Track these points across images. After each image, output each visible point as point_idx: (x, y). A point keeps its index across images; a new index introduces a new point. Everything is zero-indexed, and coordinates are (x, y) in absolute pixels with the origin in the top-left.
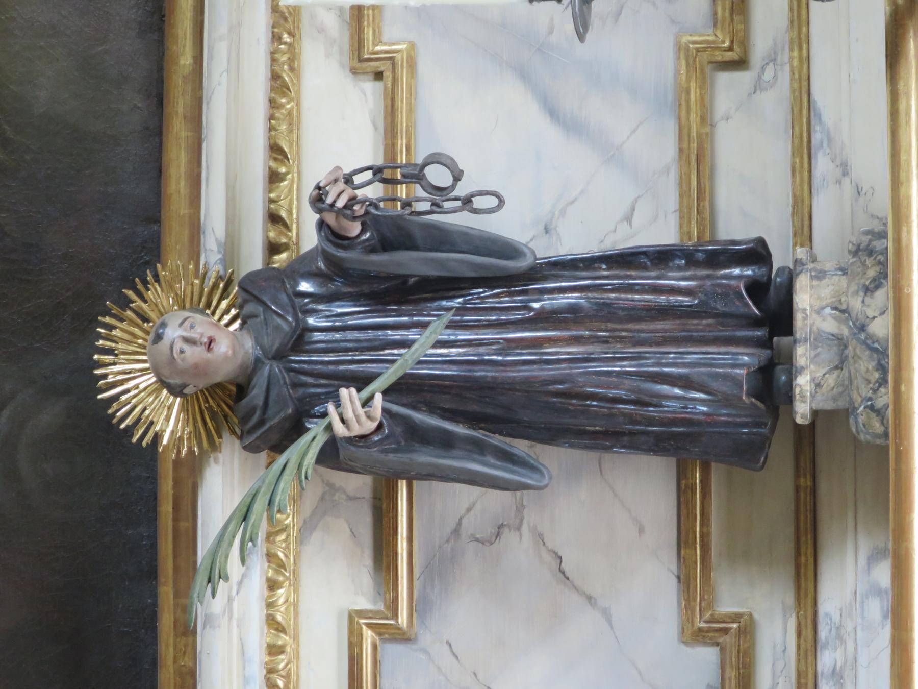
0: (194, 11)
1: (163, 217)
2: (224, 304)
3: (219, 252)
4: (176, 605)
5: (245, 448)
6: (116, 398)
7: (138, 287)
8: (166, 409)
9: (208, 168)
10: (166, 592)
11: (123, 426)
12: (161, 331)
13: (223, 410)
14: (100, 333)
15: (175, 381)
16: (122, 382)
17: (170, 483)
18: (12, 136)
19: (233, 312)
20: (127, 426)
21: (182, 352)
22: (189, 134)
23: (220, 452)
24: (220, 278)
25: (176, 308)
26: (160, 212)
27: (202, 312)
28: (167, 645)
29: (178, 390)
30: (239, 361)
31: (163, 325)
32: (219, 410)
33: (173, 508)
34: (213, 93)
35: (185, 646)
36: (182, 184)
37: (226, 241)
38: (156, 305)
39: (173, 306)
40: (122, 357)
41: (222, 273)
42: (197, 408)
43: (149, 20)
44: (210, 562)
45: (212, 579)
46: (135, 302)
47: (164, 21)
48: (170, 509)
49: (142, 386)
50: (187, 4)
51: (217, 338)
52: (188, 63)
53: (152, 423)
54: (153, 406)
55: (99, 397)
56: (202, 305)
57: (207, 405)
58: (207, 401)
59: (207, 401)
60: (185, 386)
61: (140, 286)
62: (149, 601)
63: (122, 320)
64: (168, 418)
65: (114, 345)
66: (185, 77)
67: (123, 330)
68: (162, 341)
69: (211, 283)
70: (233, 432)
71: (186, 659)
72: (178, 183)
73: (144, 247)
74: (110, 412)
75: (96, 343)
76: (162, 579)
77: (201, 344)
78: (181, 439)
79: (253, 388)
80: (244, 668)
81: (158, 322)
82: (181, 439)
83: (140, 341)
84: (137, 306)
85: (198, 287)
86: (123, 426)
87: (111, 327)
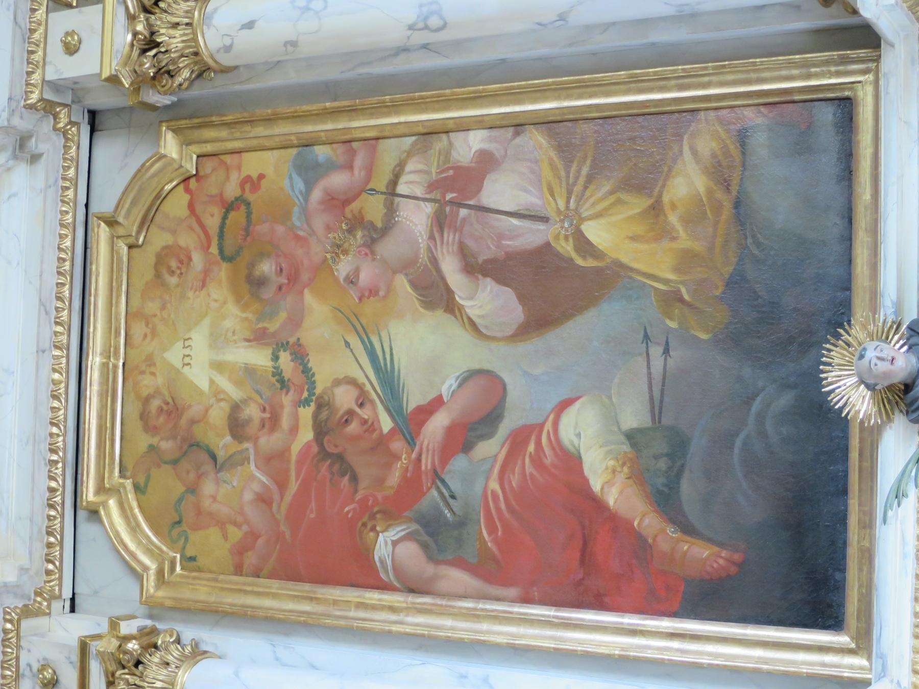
0: (871, 168)
1: (853, 287)
2: (896, 337)
3: (893, 308)
4: (860, 511)
5: (911, 421)
6: (833, 391)
7: (846, 327)
8: (862, 398)
9: (885, 259)
10: (853, 503)
11: (837, 407)
12: (863, 353)
13: (895, 399)
14: (824, 353)
15: (871, 381)
16: (836, 382)
17: (857, 440)
18: (763, 241)
19: (901, 342)
20: (839, 407)
21: (876, 365)
22: (869, 239)
23: (893, 423)
24: (893, 322)
25: (868, 339)
26: (851, 284)
27: (886, 343)
28: (853, 534)
29: (873, 387)
30: (908, 370)
31: (865, 349)
32: (893, 398)
33: (859, 455)
34: (888, 216)
35: (864, 535)
36: (865, 267)
37: (897, 301)
38: (857, 338)
39: (867, 339)
40: (836, 367)
41: (894, 319)
42: (880, 397)
43: (843, 174)
44: (897, 486)
45: (898, 497)
46: (844, 336)
47: (852, 174)
48: (857, 455)
49: (848, 384)
50: (624, 79)
51: (897, 358)
52: (867, 198)
53: (854, 405)
54: (854, 396)
55: (823, 390)
56: (883, 338)
57: (886, 396)
58: (886, 394)
59: (886, 394)
60: (876, 385)
61: (847, 327)
62: (843, 508)
63: (836, 346)
64: (863, 403)
65: (832, 360)
66: (866, 208)
67: (836, 352)
68: (864, 359)
69: (888, 326)
70: (901, 411)
71: (865, 542)
72: (862, 268)
73: (841, 305)
74: (829, 399)
75: (822, 359)
76: (850, 495)
77: (887, 360)
78: (870, 415)
79: (917, 386)
80: (904, 548)
81: (860, 349)
82: (870, 415)
83: (847, 358)
84: (845, 338)
85: (881, 328)
86: (837, 407)
87: (829, 350)
